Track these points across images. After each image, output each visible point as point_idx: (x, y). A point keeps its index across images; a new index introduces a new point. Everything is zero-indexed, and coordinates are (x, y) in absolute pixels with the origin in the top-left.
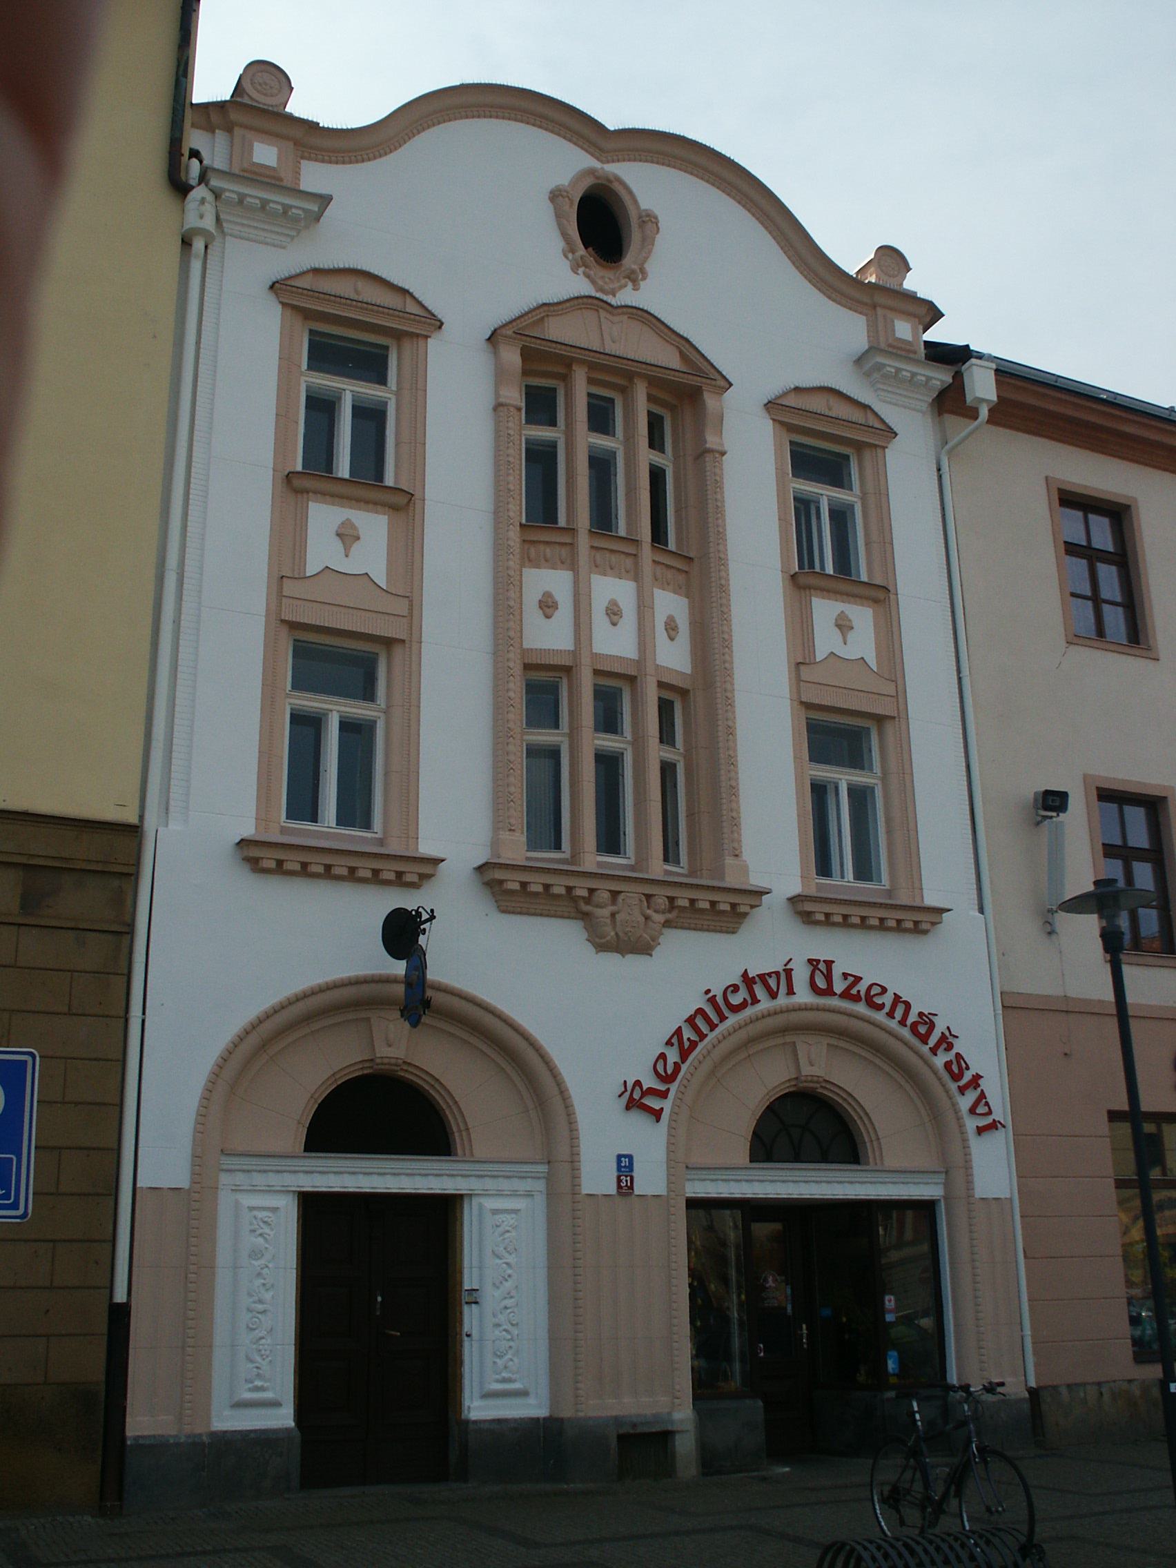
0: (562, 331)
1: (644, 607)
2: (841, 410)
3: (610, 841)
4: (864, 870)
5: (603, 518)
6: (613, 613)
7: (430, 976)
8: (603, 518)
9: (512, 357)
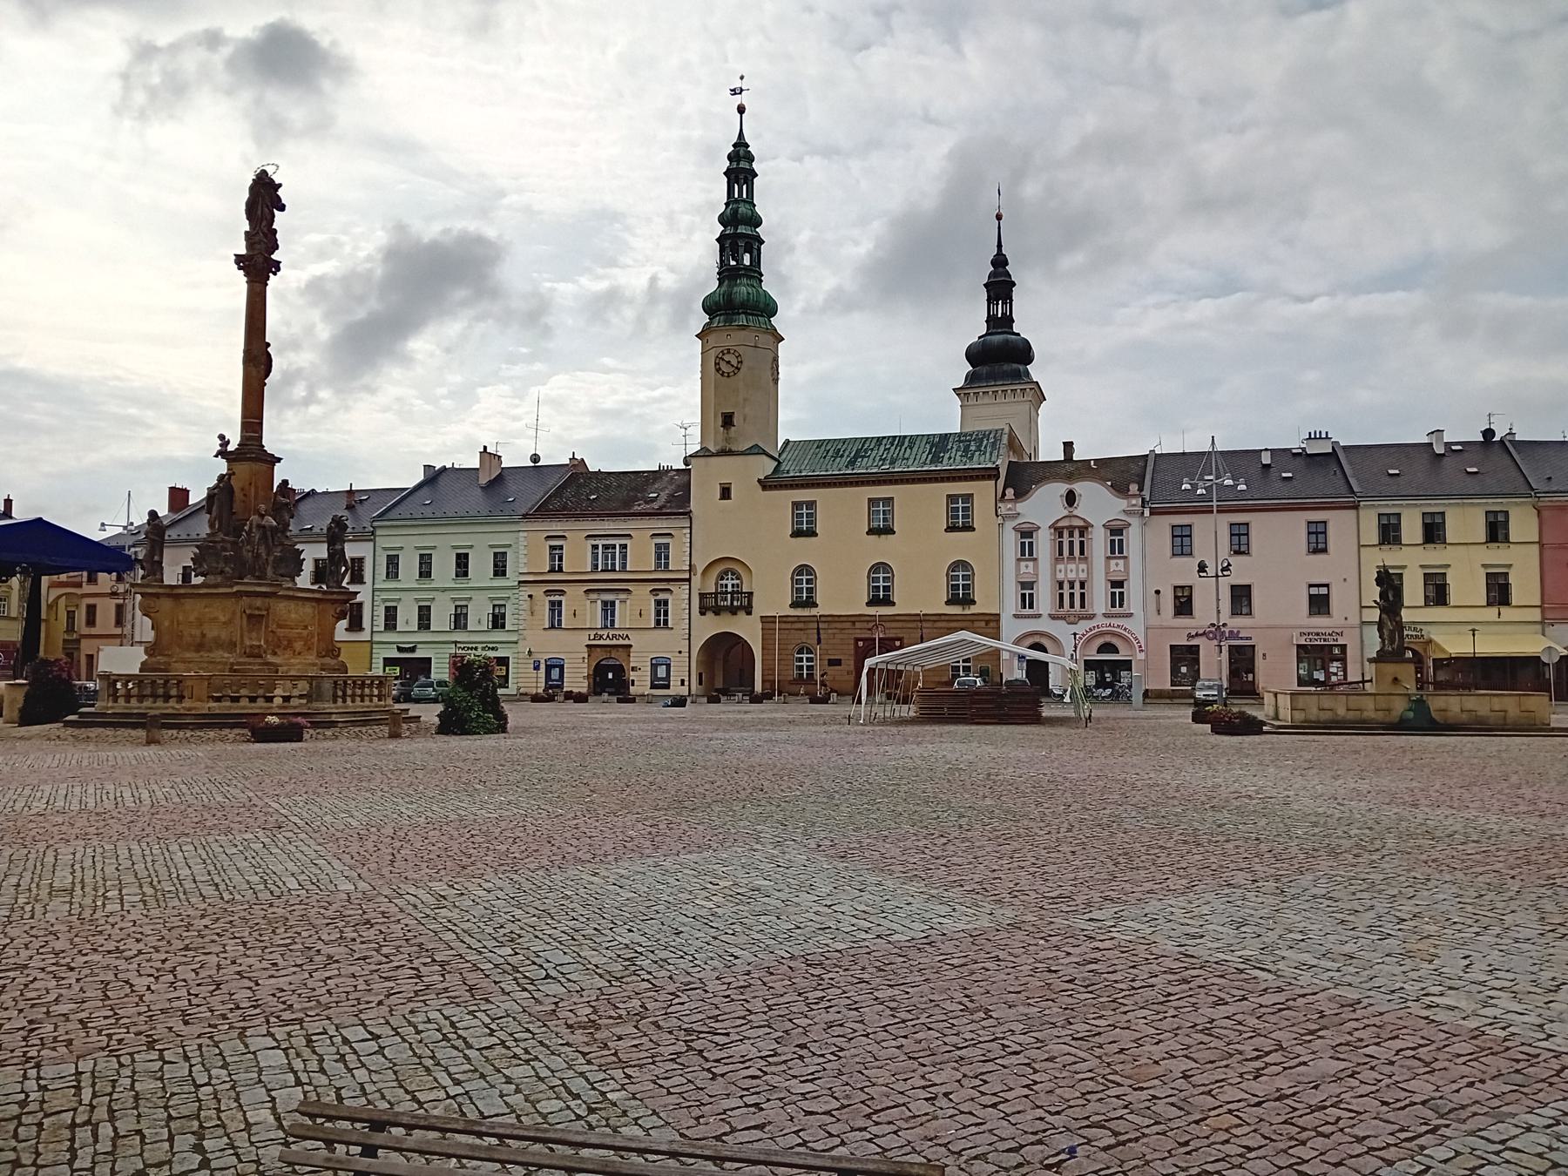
0: (1060, 524)
1: (1066, 575)
2: (1119, 523)
3: (1072, 606)
4: (1083, 606)
5: (1071, 552)
6: (1071, 571)
8: (1071, 552)
9: (1052, 530)
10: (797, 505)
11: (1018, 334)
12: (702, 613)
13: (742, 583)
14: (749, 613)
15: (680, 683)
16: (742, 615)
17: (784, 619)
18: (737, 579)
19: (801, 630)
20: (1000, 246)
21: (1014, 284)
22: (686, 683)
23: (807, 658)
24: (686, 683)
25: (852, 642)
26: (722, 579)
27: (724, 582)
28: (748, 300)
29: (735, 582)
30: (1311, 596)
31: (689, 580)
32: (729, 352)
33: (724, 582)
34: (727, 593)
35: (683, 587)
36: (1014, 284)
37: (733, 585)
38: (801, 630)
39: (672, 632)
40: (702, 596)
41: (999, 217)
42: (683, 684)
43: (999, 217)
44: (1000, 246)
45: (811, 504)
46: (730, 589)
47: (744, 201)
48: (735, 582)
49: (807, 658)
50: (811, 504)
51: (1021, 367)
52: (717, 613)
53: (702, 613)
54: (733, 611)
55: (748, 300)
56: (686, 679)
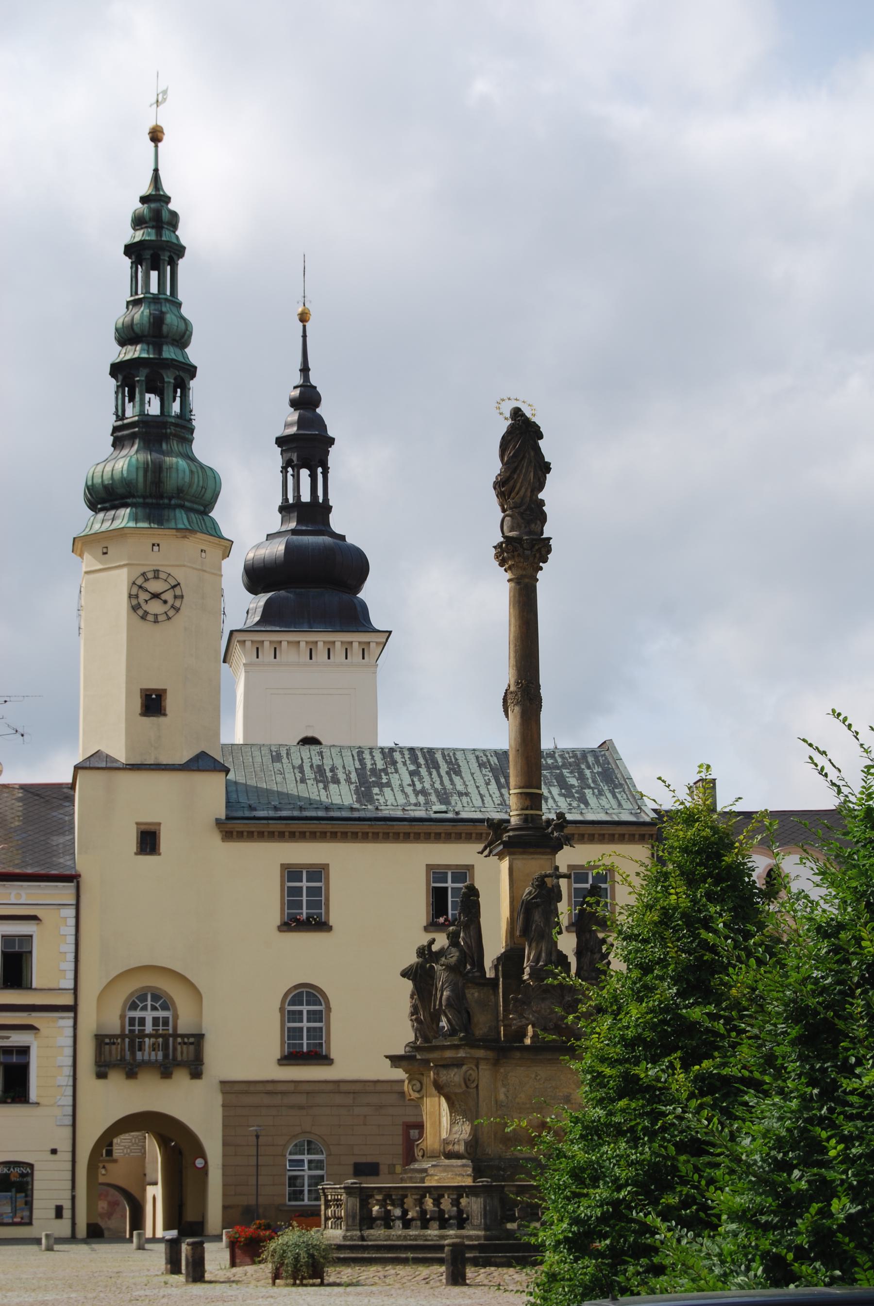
7: (118, 1032)
10: (291, 873)
11: (343, 538)
12: (101, 1075)
13: (176, 1017)
14: (196, 1074)
15: (52, 1214)
16: (181, 1078)
17: (269, 1087)
18: (165, 1007)
19: (301, 1107)
20: (305, 370)
21: (331, 441)
22: (67, 1213)
23: (310, 1162)
24: (67, 1213)
25: (399, 1130)
26: (134, 1007)
27: (137, 1014)
28: (191, 485)
29: (161, 1014)
30: (159, 1018)
31: (73, 1009)
32: (156, 577)
33: (137, 1014)
34: (142, 1035)
35: (62, 1023)
36: (331, 441)
37: (156, 1021)
38: (301, 1107)
39: (37, 1111)
40: (101, 1041)
41: (304, 318)
42: (59, 1212)
43: (304, 318)
44: (305, 370)
45: (318, 872)
46: (149, 1028)
47: (166, 300)
48: (161, 1014)
49: (310, 1162)
50: (318, 872)
51: (346, 597)
52: (131, 1074)
53: (101, 1075)
54: (166, 1071)
55: (191, 485)
56: (67, 1205)
